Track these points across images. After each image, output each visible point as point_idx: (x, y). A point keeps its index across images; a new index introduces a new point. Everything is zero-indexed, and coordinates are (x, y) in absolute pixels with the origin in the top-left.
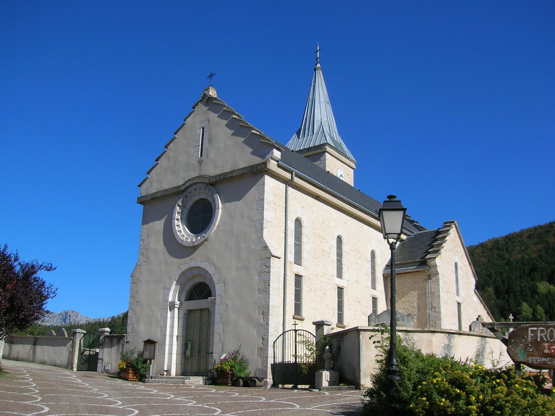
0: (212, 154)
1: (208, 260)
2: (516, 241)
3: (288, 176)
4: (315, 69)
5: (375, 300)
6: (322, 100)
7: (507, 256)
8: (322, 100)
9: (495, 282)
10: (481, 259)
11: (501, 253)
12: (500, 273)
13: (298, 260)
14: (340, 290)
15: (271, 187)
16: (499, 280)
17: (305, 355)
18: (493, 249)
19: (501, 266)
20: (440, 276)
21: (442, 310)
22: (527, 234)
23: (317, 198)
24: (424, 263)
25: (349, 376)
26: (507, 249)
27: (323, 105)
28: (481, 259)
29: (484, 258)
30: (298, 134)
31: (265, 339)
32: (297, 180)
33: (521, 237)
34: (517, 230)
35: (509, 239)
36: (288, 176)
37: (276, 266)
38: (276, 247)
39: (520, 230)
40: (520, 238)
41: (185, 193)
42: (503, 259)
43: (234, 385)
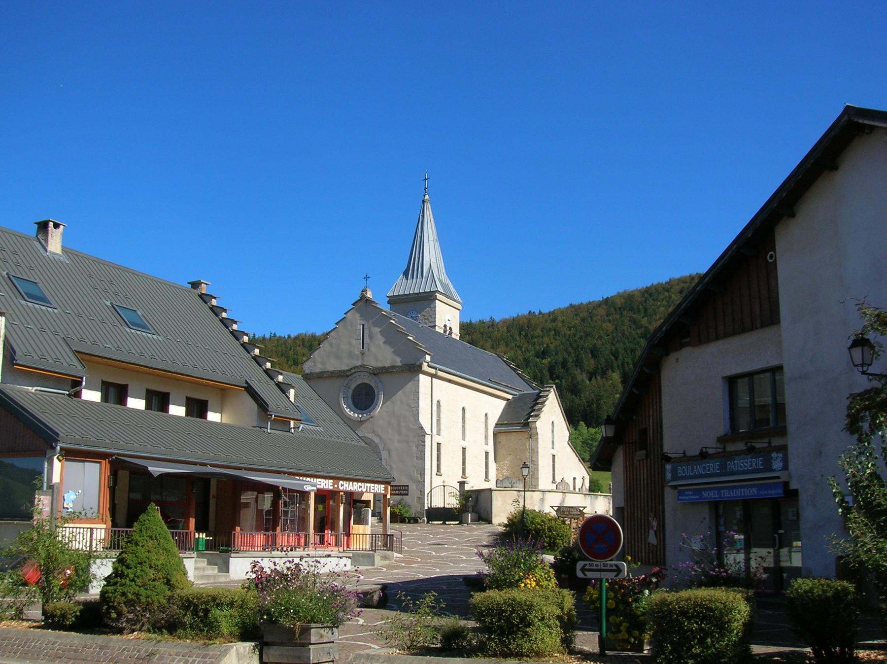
0: (373, 349)
1: (374, 432)
2: (661, 297)
3: (433, 371)
4: (423, 201)
5: (487, 453)
6: (431, 238)
7: (644, 322)
8: (431, 238)
9: (622, 364)
10: (604, 325)
11: (635, 316)
12: (632, 351)
13: (438, 434)
14: (464, 449)
15: (424, 380)
16: (630, 361)
17: (453, 502)
18: (624, 309)
19: (634, 339)
20: (539, 436)
21: (540, 463)
22: (678, 288)
23: (450, 381)
24: (526, 425)
25: (484, 516)
26: (646, 310)
27: (432, 243)
28: (604, 325)
29: (609, 324)
30: (406, 274)
31: (422, 492)
32: (440, 373)
33: (668, 291)
34: (663, 279)
35: (650, 295)
36: (433, 371)
37: (428, 439)
38: (427, 429)
39: (668, 280)
40: (666, 294)
41: (350, 378)
42: (639, 327)
43: (401, 522)
